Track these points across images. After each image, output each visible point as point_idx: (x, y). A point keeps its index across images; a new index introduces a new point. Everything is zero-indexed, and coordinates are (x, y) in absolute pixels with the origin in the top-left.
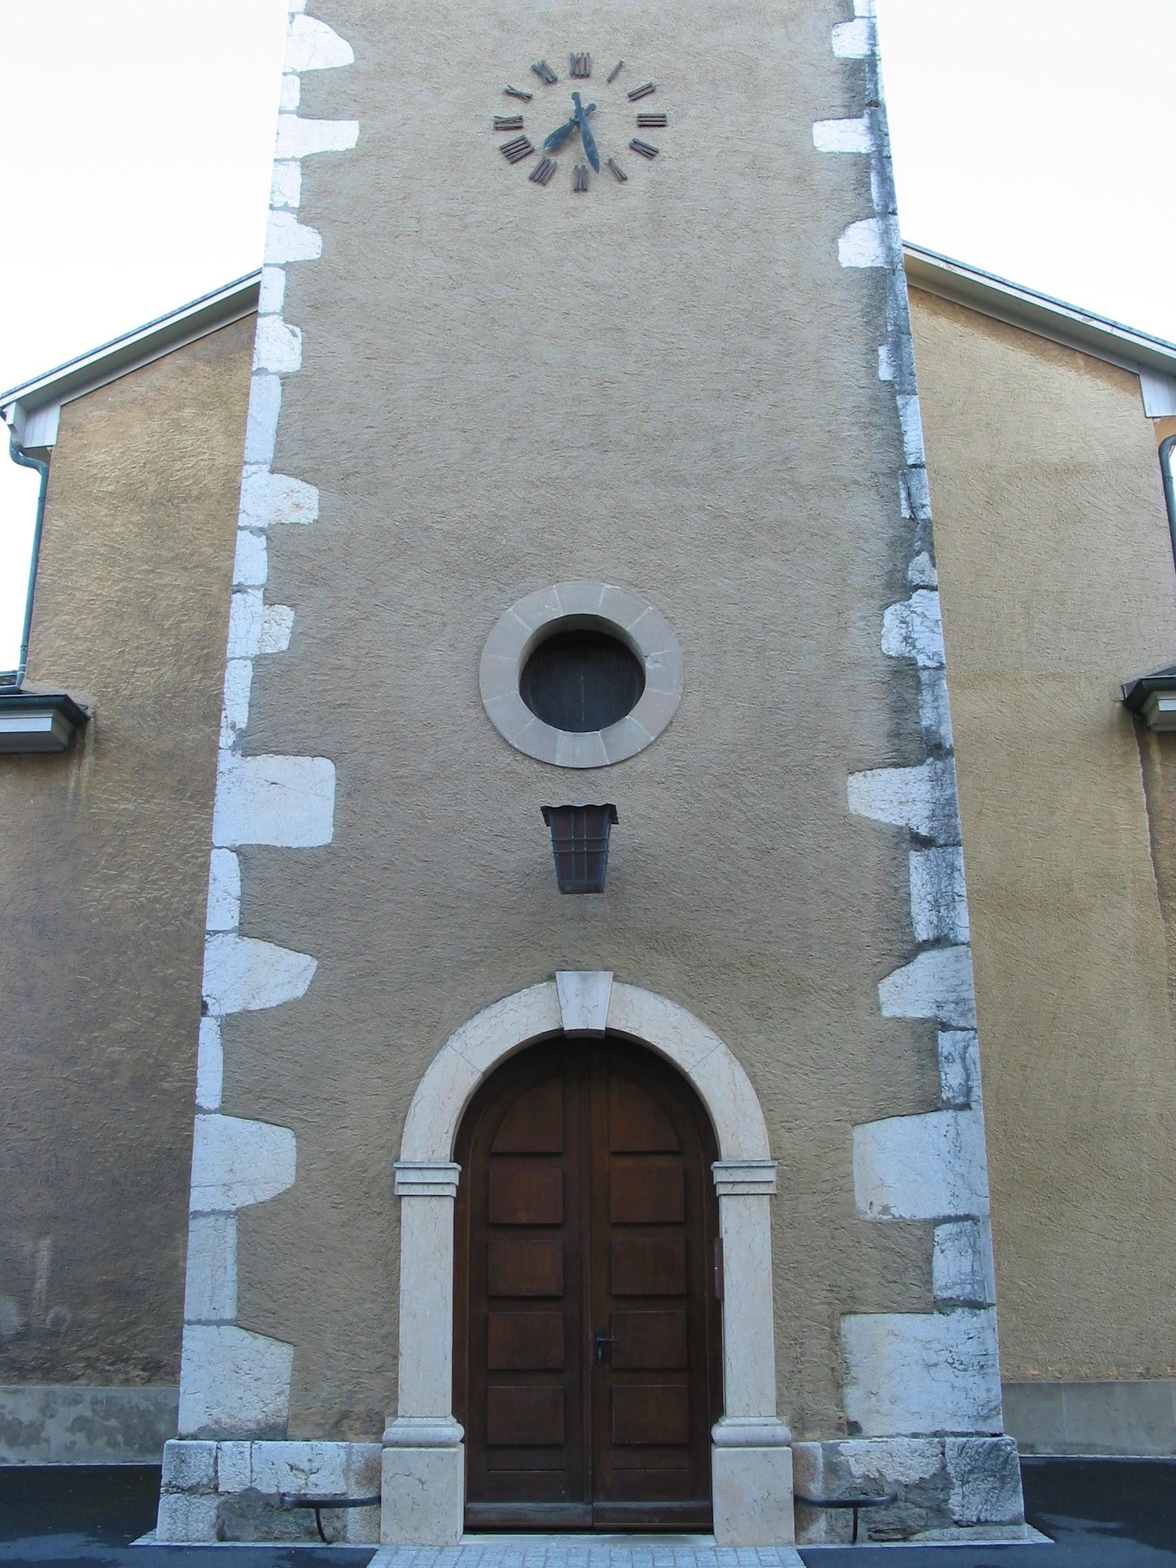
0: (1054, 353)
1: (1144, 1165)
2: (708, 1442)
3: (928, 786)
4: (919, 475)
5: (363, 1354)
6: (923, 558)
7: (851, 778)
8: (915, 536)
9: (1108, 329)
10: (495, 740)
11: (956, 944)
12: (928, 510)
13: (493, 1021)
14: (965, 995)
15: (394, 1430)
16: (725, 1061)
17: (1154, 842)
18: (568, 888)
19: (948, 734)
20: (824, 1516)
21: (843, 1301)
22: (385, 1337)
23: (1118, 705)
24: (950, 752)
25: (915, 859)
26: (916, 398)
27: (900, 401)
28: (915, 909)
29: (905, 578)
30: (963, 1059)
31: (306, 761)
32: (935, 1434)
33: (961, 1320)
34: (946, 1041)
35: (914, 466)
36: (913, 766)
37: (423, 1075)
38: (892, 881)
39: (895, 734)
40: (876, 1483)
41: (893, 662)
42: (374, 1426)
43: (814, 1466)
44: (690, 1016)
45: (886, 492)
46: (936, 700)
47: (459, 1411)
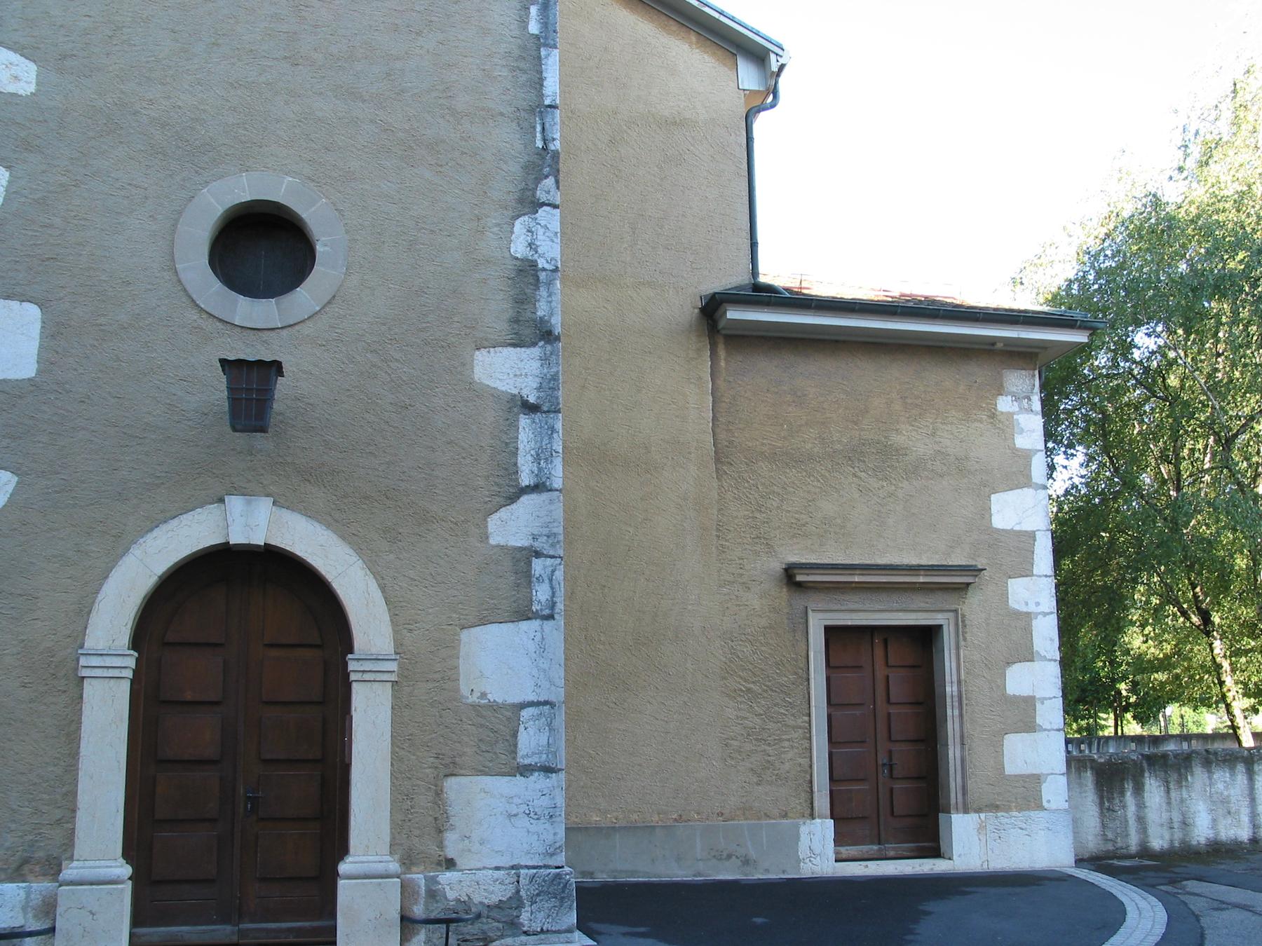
0: (674, 28)
1: (689, 665)
2: (335, 875)
3: (538, 364)
4: (553, 114)
5: (45, 809)
6: (550, 182)
7: (477, 353)
8: (544, 163)
9: (716, 15)
10: (184, 299)
11: (551, 490)
12: (557, 143)
13: (170, 534)
14: (555, 530)
15: (69, 871)
16: (361, 573)
17: (714, 419)
18: (239, 427)
19: (557, 323)
20: (423, 931)
21: (446, 766)
22: (66, 794)
23: (697, 311)
24: (558, 338)
25: (524, 421)
26: (556, 52)
27: (543, 52)
28: (520, 460)
29: (534, 196)
30: (551, 580)
31: (15, 304)
32: (513, 867)
33: (537, 781)
34: (538, 566)
35: (550, 106)
36: (528, 347)
37: (107, 577)
38: (504, 437)
39: (516, 321)
40: (466, 904)
41: (518, 263)
42: (53, 868)
43: (418, 892)
44: (335, 537)
45: (526, 125)
46: (550, 296)
47: (127, 855)
